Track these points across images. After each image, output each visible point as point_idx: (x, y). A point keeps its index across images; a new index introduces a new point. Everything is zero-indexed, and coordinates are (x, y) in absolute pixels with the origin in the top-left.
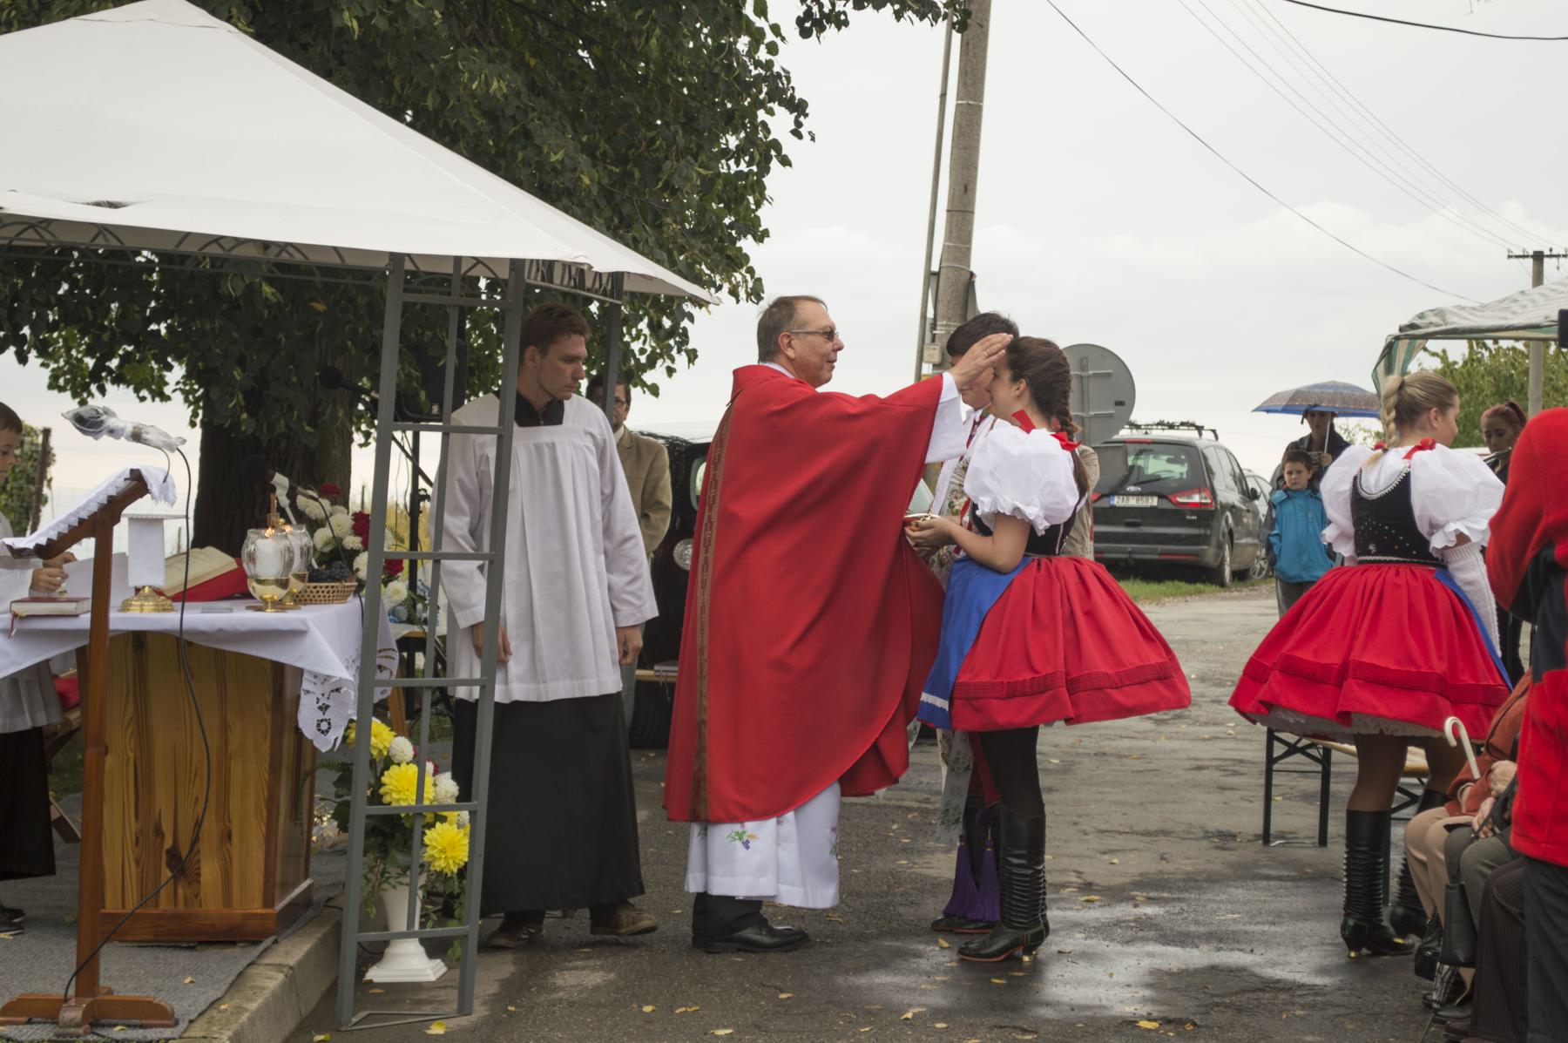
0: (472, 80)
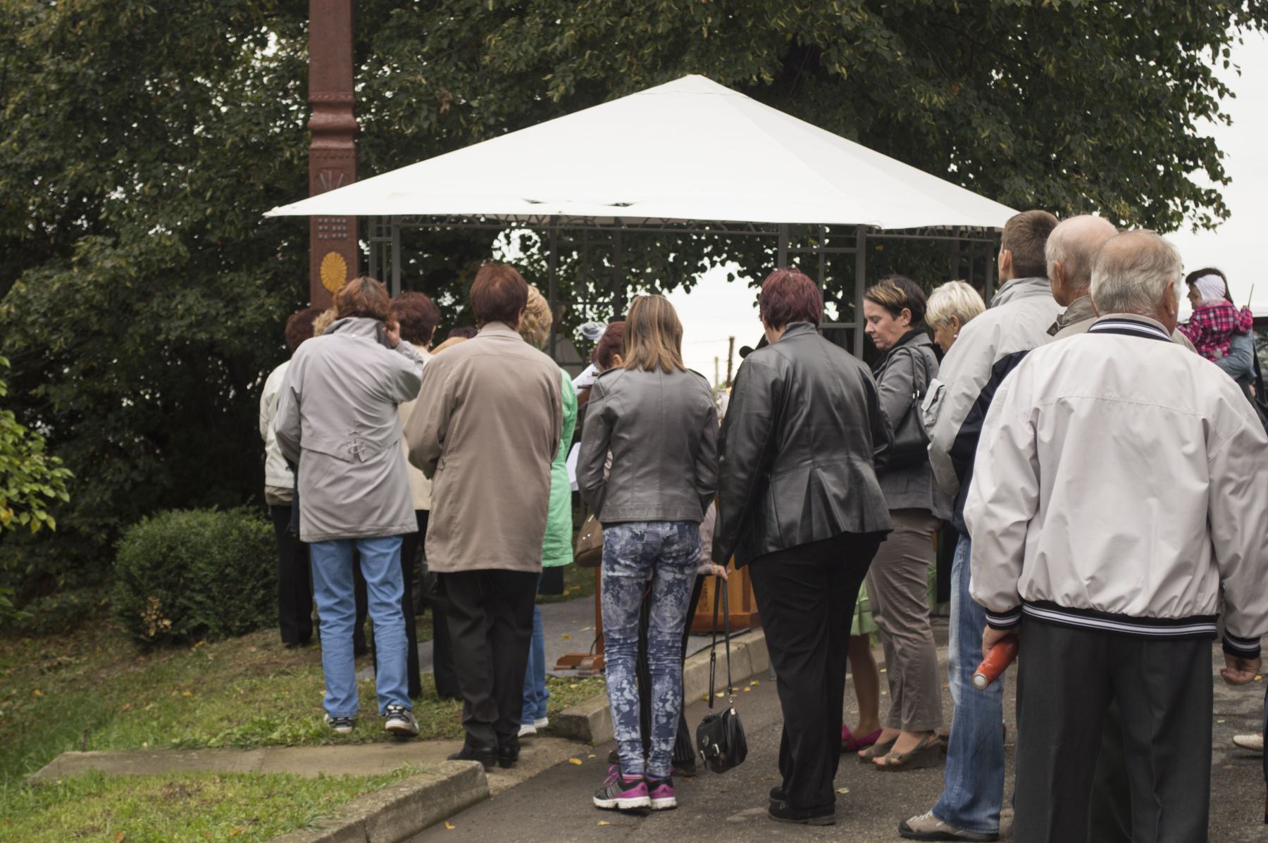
0: (920, 98)
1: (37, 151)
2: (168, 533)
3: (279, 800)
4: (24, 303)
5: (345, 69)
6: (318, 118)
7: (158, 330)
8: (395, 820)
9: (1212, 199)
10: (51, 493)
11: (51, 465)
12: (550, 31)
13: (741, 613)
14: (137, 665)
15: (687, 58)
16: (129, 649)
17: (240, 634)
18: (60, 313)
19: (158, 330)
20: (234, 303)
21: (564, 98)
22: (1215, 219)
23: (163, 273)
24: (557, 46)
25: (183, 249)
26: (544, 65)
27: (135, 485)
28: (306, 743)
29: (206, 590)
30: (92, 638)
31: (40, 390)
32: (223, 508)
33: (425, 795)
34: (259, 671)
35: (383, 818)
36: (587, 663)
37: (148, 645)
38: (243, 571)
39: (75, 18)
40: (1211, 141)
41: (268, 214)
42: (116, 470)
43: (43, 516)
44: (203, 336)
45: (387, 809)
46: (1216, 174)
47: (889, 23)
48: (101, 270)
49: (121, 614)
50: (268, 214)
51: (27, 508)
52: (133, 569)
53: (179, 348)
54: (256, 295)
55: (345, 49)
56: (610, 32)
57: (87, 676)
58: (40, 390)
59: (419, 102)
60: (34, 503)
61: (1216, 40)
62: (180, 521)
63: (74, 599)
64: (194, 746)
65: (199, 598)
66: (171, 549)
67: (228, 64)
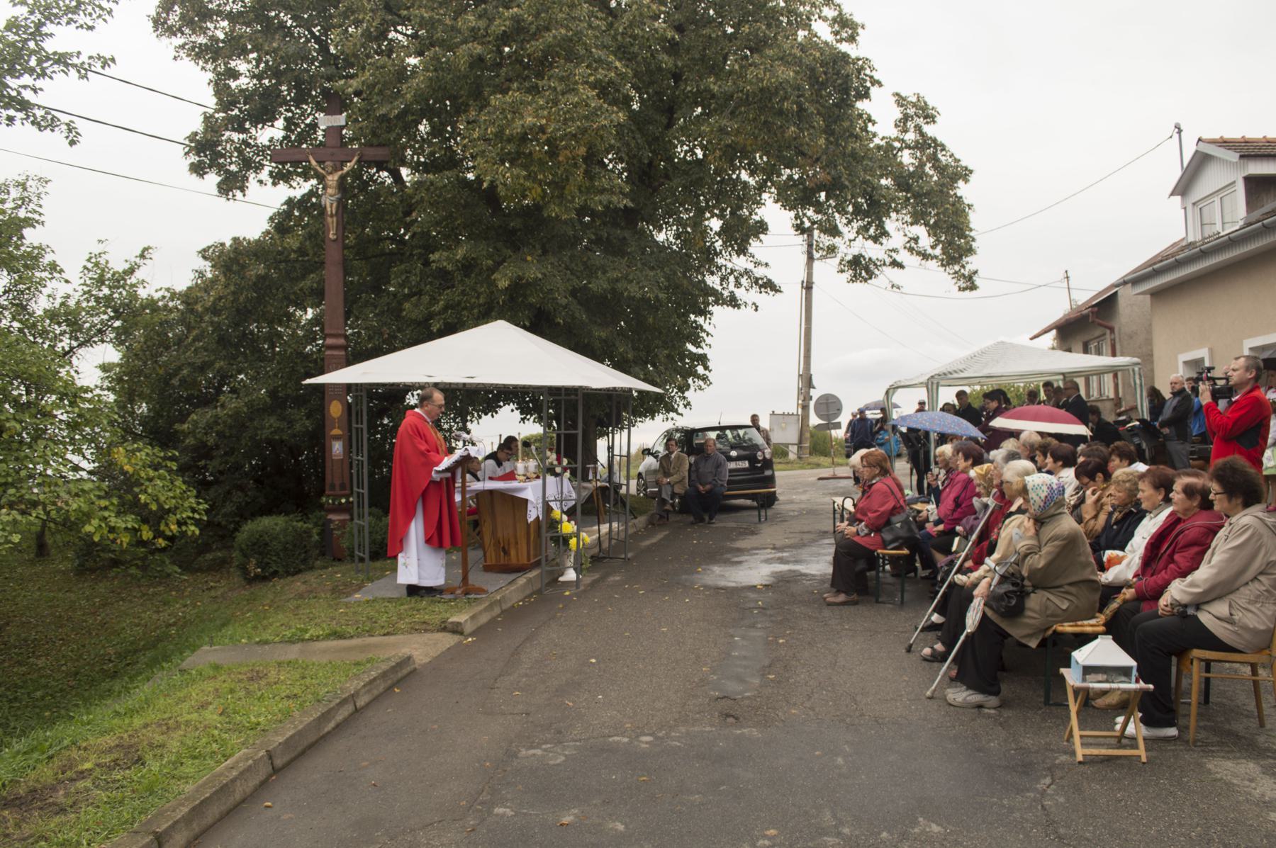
1: (204, 357)
2: (260, 529)
3: (308, 681)
4: (195, 423)
5: (342, 320)
6: (330, 341)
7: (256, 435)
8: (369, 691)
9: (704, 378)
10: (197, 516)
11: (199, 503)
12: (434, 300)
13: (526, 562)
14: (245, 589)
15: (493, 314)
16: (243, 583)
17: (293, 575)
18: (212, 428)
19: (256, 435)
20: (291, 423)
21: (439, 330)
22: (703, 386)
23: (258, 410)
24: (436, 308)
25: (268, 399)
26: (431, 316)
27: (247, 503)
28: (323, 639)
29: (277, 555)
30: (228, 572)
31: (202, 463)
32: (287, 514)
33: (384, 675)
34: (301, 596)
35: (363, 691)
36: (459, 592)
37: (251, 580)
38: (295, 546)
39: (220, 298)
40: (705, 355)
41: (304, 382)
42: (238, 497)
43: (193, 528)
44: (277, 437)
45: (364, 686)
46: (706, 368)
47: (580, 303)
48: (230, 409)
49: (238, 566)
50: (304, 382)
51: (186, 524)
52: (243, 546)
53: (270, 442)
54: (301, 419)
55: (341, 311)
56: (459, 303)
57: (222, 594)
58: (202, 463)
59: (374, 333)
60: (189, 521)
61: (704, 313)
62: (266, 522)
63: (219, 554)
64: (266, 642)
65: (274, 558)
66: (261, 536)
67: (289, 320)
